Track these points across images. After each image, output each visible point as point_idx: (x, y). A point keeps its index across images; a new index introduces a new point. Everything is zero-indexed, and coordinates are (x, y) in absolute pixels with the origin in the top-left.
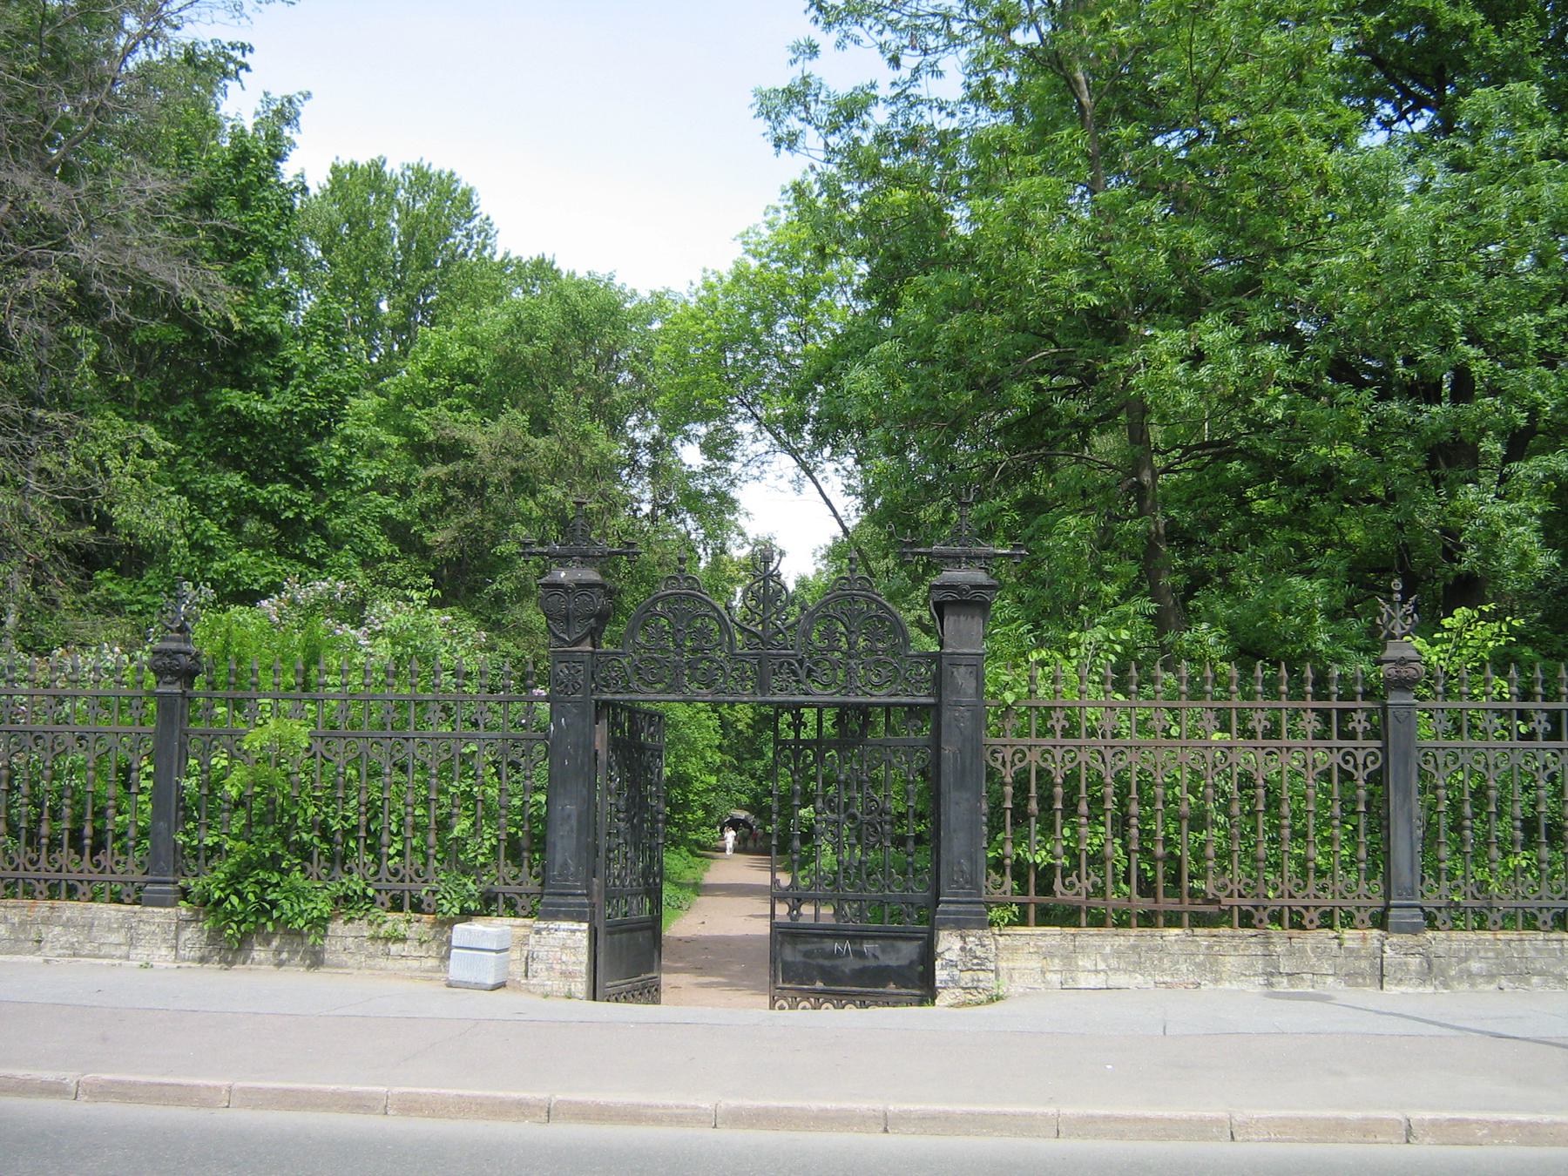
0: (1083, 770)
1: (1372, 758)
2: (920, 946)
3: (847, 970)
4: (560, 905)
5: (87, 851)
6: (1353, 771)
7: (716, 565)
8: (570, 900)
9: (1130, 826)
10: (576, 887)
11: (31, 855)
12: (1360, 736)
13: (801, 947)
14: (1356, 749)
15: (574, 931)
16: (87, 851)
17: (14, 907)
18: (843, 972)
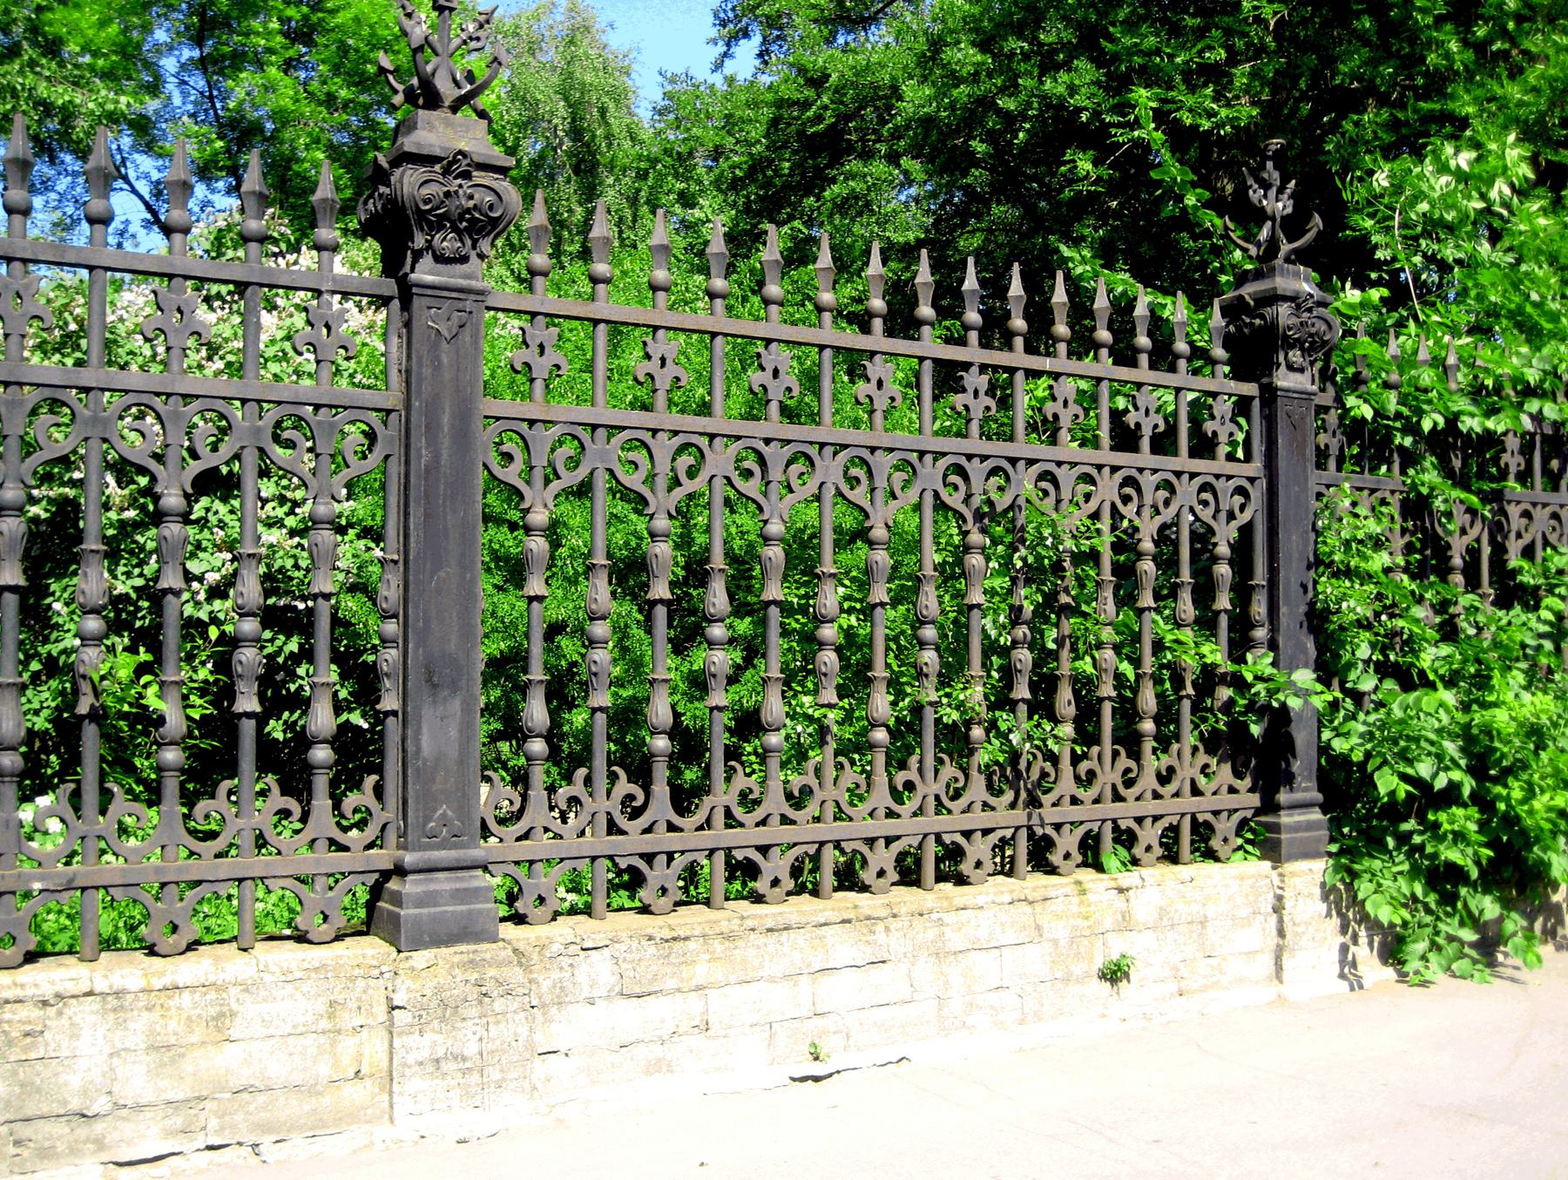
1: (691, 460)
5: (321, 782)
12: (1145, 443)
16: (321, 782)
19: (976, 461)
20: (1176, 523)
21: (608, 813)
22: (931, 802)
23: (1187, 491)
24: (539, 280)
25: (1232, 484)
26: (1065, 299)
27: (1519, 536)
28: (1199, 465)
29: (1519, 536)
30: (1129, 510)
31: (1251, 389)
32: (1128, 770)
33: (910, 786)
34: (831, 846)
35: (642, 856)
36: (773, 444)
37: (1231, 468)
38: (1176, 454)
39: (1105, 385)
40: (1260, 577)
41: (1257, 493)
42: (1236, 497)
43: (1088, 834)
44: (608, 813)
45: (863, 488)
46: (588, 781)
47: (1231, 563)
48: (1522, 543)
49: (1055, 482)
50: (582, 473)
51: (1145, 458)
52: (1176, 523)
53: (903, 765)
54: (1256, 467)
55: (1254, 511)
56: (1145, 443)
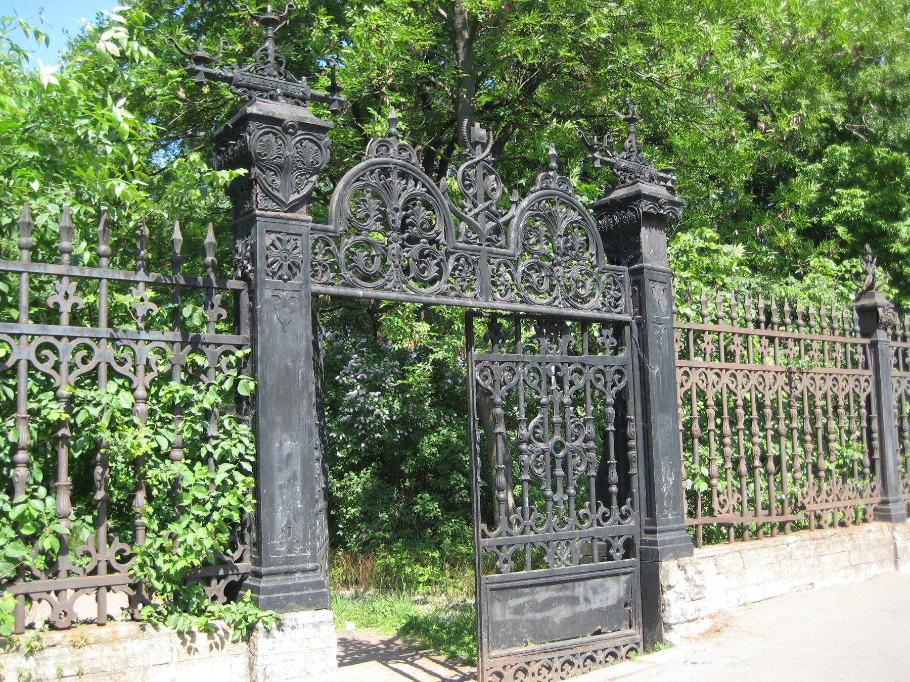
0: (521, 388)
1: (84, 352)
2: (627, 582)
3: (557, 620)
4: (287, 589)
5: (614, 499)
6: (53, 373)
7: (180, 77)
8: (299, 578)
9: (629, 449)
10: (305, 560)
11: (603, 509)
12: (65, 318)
13: (514, 602)
14: (59, 338)
15: (317, 625)
16: (614, 499)
17: (753, 549)
18: (554, 623)
19: (65, 340)
20: (690, 390)
21: (107, 561)
22: (595, 522)
23: (726, 377)
24: (720, 321)
25: (572, 367)
26: (213, 240)
27: (682, 386)
28: (728, 365)
29: (843, 390)
30: (835, 389)
31: (867, 341)
32: (605, 513)
33: (586, 516)
34: (105, 589)
35: (544, 542)
36: (211, 346)
37: (742, 366)
38: (58, 323)
39: (722, 335)
40: (874, 414)
41: (872, 380)
42: (616, 376)
43: (516, 552)
44: (107, 561)
45: (129, 366)
46: (632, 504)
47: (614, 406)
48: (844, 393)
49: (735, 377)
50: (91, 365)
51: (860, 371)
52: (690, 390)
53: (582, 507)
54: (870, 372)
55: (871, 389)
56: (65, 318)
